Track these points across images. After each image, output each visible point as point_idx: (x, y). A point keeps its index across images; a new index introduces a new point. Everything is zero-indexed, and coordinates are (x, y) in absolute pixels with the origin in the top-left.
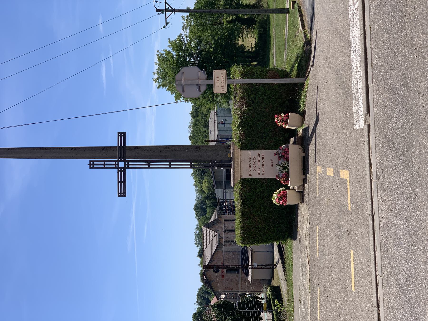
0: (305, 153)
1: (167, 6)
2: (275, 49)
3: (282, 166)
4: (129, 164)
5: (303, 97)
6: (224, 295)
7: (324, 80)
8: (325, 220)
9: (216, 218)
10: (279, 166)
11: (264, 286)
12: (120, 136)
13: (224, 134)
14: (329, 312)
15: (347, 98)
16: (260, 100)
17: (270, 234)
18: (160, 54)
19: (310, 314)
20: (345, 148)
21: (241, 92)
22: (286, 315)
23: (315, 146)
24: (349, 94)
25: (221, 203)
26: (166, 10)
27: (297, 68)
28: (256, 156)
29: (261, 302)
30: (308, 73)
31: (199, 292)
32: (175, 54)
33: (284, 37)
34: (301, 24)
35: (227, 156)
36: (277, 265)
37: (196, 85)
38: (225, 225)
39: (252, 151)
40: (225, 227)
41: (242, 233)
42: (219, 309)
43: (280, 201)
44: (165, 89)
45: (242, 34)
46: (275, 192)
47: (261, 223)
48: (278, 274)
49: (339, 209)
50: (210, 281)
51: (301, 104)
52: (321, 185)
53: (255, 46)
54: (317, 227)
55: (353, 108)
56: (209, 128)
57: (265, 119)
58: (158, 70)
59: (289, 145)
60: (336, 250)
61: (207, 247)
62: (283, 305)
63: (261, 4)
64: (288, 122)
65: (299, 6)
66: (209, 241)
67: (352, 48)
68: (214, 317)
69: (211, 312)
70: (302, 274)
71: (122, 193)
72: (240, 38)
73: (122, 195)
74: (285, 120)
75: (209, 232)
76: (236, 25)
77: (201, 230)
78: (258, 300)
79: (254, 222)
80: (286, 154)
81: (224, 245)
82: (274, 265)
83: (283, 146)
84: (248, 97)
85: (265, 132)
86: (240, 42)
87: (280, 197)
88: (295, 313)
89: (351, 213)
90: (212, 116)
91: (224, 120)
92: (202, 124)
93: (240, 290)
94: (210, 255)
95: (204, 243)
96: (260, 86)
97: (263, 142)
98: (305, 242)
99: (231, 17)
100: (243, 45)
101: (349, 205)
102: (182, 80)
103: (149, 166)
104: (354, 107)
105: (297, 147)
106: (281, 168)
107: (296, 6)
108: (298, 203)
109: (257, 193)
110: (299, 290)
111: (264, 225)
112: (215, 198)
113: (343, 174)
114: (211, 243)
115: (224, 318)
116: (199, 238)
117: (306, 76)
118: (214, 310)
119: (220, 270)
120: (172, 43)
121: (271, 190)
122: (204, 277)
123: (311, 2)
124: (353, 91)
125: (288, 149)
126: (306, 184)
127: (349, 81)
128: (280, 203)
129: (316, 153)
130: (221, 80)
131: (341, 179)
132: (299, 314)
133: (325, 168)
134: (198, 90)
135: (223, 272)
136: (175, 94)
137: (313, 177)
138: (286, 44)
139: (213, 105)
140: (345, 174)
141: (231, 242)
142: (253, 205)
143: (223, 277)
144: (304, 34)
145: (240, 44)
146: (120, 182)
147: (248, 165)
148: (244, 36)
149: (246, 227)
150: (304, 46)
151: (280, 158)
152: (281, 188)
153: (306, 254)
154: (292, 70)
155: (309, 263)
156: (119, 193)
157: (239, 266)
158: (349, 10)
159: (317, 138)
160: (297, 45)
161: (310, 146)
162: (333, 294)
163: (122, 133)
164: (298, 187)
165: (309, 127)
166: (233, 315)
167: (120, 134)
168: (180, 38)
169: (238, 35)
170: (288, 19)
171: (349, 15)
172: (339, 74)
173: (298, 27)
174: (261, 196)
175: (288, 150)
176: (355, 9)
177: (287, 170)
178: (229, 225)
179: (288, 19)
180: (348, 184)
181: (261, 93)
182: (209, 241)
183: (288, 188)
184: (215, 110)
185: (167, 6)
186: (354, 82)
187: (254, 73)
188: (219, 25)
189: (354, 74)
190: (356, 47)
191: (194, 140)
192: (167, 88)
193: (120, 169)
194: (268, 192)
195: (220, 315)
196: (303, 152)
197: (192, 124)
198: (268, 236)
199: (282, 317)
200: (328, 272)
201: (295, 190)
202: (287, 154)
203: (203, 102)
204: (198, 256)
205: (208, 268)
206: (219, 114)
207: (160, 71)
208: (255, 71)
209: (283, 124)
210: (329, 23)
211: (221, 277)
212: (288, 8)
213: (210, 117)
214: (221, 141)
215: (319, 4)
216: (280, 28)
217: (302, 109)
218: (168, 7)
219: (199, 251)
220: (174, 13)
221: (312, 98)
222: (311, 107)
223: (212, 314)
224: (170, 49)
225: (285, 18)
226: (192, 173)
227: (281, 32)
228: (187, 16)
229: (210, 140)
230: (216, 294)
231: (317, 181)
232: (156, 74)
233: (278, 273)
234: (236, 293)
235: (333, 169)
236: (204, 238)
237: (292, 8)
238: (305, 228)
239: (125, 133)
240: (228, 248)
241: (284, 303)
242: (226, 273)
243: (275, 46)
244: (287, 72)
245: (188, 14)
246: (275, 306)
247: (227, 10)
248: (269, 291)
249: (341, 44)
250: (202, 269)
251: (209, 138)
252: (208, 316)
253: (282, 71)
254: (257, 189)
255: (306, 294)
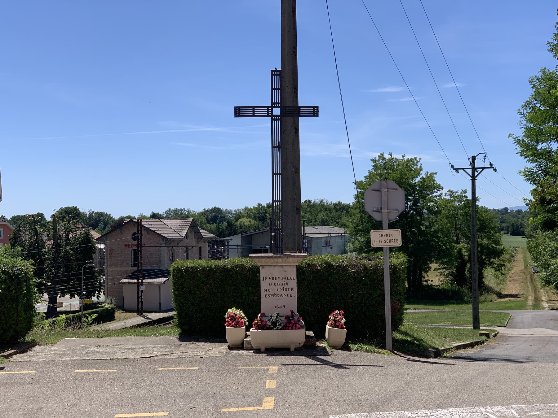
0: (294, 350)
1: (480, 170)
2: (426, 311)
3: (276, 320)
4: (278, 121)
5: (368, 347)
6: (102, 248)
7: (391, 374)
8: (208, 378)
9: (203, 236)
10: (277, 317)
11: (115, 300)
12: (314, 109)
13: (314, 245)
14: (86, 384)
15: (370, 406)
16: (362, 291)
17: (186, 306)
18: (417, 162)
19: (82, 359)
20: (303, 403)
21: (372, 266)
22: (78, 329)
23: (304, 363)
24: (374, 408)
25: (222, 243)
26: (474, 169)
27: (404, 340)
28: (289, 287)
29: (94, 296)
30: (400, 354)
31: (106, 214)
32: (417, 181)
33: (441, 323)
34: (461, 345)
35: (288, 249)
36: (143, 317)
37: (381, 207)
38: (194, 248)
39: (295, 281)
40: (193, 247)
41: (188, 269)
42: (85, 241)
43: (230, 319)
44: (371, 168)
45: (444, 268)
46: (242, 311)
47: (201, 294)
48: (130, 318)
49: (223, 395)
50: (121, 228)
51: (359, 344)
52: (253, 371)
53: (428, 285)
54: (198, 368)
55: (357, 413)
56: (322, 227)
57: (337, 297)
58: (395, 159)
59: (304, 330)
60: (167, 392)
61: (166, 224)
62: (91, 324)
63: (484, 292)
64: (334, 327)
65: (483, 342)
66: (173, 227)
67: (436, 411)
68: (74, 235)
69: (81, 230)
70: (134, 349)
71: (239, 112)
72: (438, 266)
73: (237, 112)
74: (337, 324)
75: (186, 227)
76: (456, 260)
77: (187, 217)
78: (97, 292)
79: (203, 285)
80: (293, 325)
81: (168, 247)
82: (142, 313)
83: (302, 321)
84: (366, 275)
85: (320, 298)
86: (433, 266)
87: (236, 319)
88: (82, 339)
89: (219, 413)
90: (336, 230)
91: (332, 245)
92: (326, 217)
93: (109, 268)
94: (155, 228)
95: (171, 221)
96: (380, 291)
97: (307, 295)
98: (177, 352)
99: (466, 254)
100: (430, 270)
101: (228, 409)
102: (387, 189)
103: (275, 147)
104: (358, 414)
105: (302, 340)
106: (274, 319)
107: (484, 338)
108: (228, 343)
109: (241, 289)
110: (113, 345)
111: (198, 298)
112: (230, 235)
113: (269, 400)
114: (171, 229)
115: (72, 248)
116: (177, 215)
117: (395, 352)
118: (83, 234)
119: (136, 242)
120: (430, 177)
121: (245, 306)
122: (126, 222)
123: (491, 357)
124: (379, 413)
125: (299, 329)
126: (253, 352)
127: (392, 407)
128: (228, 318)
129: (295, 365)
130: (389, 240)
131: (262, 398)
132: (82, 345)
133: (275, 378)
134: (375, 209)
135: (133, 246)
136: (365, 181)
137: (263, 361)
138: (433, 325)
139: (351, 230)
140: (269, 403)
141: (173, 256)
142: (225, 283)
143: (126, 246)
144: (449, 349)
145: (431, 265)
146: (254, 110)
147: (277, 276)
148: (441, 270)
149: (196, 275)
150: (433, 348)
151: (287, 317)
152: (247, 319)
153: (161, 354)
154: (402, 333)
155: (150, 357)
156: (239, 108)
157: (141, 266)
158: (485, 406)
159: (315, 366)
160: (435, 339)
161: (304, 357)
162: (109, 390)
163: (318, 111)
164: (249, 342)
165: (329, 355)
166: (77, 260)
167: (316, 109)
168: (438, 188)
169: (442, 263)
170: (466, 327)
171: (478, 407)
172: (401, 394)
173: (457, 341)
174: (237, 293)
175: (298, 328)
176: (487, 414)
177: (271, 326)
178: (194, 252)
179: (466, 327)
180: (256, 408)
181: (371, 292)
182: (173, 227)
183: (248, 329)
184: (345, 234)
185: (480, 170)
186: (392, 415)
187: (397, 283)
188: (455, 238)
189: (401, 414)
190: (437, 416)
191: (305, 206)
192: (373, 171)
193: (270, 109)
194: (242, 302)
195: (77, 242)
196: (295, 348)
197: (326, 204)
198: (184, 303)
199: (75, 324)
200: (138, 383)
201: (246, 338)
202: (293, 327)
203: (355, 219)
204: (153, 213)
205: (138, 225)
206: (339, 239)
207: (395, 162)
208: (400, 284)
209: (332, 322)
210: (467, 380)
211: (126, 243)
212: (480, 328)
213: (335, 227)
214: (304, 241)
215: (491, 367)
216: (454, 318)
217: (352, 346)
218: (478, 172)
219: (160, 214)
220: (471, 179)
221: (366, 359)
222: (355, 358)
223: (78, 232)
224: (423, 174)
225: (467, 323)
226: (261, 205)
227: (448, 320)
228: (466, 197)
229: (306, 227)
230: (104, 237)
231: (257, 367)
232: (390, 156)
233: (132, 318)
234: (106, 263)
235: (275, 387)
236: (177, 221)
237: (480, 333)
238: (195, 351)
239: (317, 116)
240: (165, 252)
241: (93, 325)
242: (132, 250)
243: (430, 312)
244: (400, 326)
245: (470, 197)
246: (90, 314)
247: (475, 248)
248: (108, 306)
249: (440, 396)
250: (136, 218)
251: (308, 226)
252: (76, 227)
253: (401, 320)
254: (245, 287)
255: (108, 354)
